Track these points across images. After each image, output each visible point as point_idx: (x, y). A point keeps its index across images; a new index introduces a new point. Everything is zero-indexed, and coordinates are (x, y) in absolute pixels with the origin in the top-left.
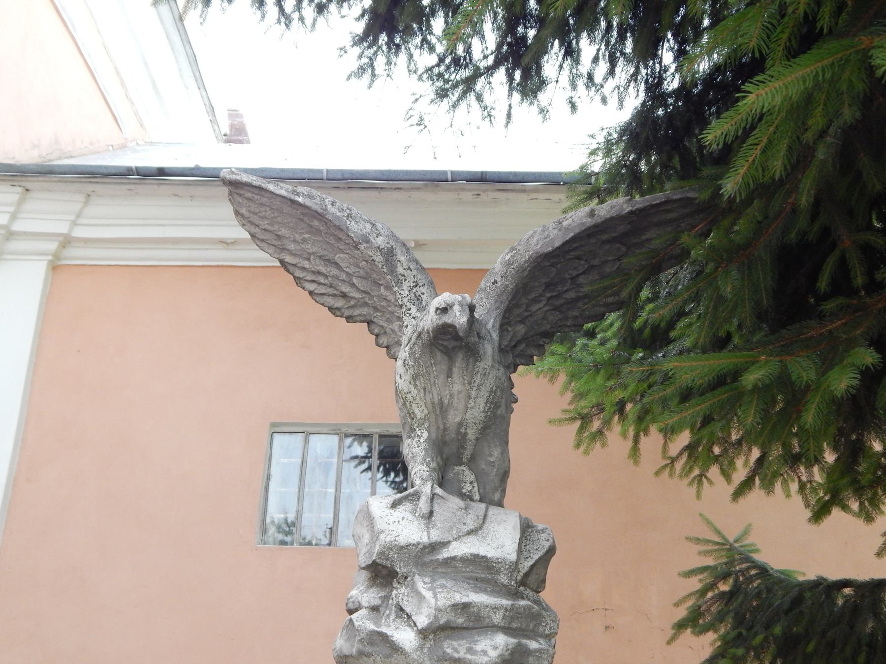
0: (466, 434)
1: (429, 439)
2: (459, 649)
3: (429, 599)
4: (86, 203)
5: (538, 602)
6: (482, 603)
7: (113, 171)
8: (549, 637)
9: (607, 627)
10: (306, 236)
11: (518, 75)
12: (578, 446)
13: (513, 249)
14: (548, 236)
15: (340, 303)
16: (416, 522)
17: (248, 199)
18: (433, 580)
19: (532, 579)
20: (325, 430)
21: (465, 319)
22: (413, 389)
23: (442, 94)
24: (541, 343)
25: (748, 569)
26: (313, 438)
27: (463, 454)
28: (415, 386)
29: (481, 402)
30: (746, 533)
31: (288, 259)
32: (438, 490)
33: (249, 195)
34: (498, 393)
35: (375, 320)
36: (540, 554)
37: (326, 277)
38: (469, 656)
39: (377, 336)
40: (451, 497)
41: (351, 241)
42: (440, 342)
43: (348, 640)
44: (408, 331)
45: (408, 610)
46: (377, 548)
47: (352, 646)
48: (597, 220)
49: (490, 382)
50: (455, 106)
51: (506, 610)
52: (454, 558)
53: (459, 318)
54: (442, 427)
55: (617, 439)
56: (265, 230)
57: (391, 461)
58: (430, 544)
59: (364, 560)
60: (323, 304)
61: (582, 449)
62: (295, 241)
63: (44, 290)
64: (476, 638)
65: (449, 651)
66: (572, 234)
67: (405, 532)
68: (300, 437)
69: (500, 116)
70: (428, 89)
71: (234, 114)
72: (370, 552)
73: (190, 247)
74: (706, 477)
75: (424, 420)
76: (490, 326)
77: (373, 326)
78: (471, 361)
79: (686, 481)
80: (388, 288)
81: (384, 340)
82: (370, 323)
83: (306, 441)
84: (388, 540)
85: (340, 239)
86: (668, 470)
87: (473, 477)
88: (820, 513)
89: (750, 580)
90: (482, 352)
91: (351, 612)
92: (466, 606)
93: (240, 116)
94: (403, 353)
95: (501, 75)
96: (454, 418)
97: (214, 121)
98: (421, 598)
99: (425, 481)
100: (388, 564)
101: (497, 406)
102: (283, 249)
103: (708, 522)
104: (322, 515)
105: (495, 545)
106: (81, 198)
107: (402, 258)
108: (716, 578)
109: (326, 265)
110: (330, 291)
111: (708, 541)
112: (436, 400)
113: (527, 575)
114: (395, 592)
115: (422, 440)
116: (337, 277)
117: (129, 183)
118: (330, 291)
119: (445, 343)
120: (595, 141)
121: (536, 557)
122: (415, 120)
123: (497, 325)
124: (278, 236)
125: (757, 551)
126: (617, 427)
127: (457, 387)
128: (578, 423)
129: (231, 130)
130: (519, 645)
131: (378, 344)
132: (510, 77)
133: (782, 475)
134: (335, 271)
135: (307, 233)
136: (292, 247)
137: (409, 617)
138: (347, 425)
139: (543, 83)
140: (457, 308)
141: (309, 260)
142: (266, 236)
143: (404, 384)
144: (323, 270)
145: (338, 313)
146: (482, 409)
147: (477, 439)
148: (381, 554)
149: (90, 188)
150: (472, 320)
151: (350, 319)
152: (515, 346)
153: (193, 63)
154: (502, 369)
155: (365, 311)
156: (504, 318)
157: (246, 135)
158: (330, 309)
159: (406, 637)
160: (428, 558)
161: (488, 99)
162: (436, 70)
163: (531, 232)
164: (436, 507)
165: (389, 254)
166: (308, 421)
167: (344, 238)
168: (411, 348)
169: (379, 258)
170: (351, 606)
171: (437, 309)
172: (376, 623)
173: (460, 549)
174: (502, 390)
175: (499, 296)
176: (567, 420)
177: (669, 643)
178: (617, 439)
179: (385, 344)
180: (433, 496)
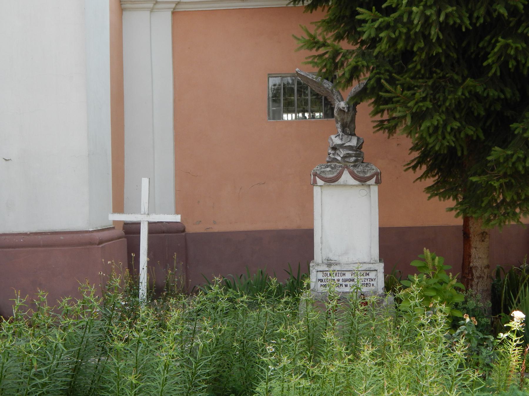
5: (360, 151)
9: (398, 145)
59: (331, 146)
96: (345, 121)
159: (339, 158)
173: (347, 144)
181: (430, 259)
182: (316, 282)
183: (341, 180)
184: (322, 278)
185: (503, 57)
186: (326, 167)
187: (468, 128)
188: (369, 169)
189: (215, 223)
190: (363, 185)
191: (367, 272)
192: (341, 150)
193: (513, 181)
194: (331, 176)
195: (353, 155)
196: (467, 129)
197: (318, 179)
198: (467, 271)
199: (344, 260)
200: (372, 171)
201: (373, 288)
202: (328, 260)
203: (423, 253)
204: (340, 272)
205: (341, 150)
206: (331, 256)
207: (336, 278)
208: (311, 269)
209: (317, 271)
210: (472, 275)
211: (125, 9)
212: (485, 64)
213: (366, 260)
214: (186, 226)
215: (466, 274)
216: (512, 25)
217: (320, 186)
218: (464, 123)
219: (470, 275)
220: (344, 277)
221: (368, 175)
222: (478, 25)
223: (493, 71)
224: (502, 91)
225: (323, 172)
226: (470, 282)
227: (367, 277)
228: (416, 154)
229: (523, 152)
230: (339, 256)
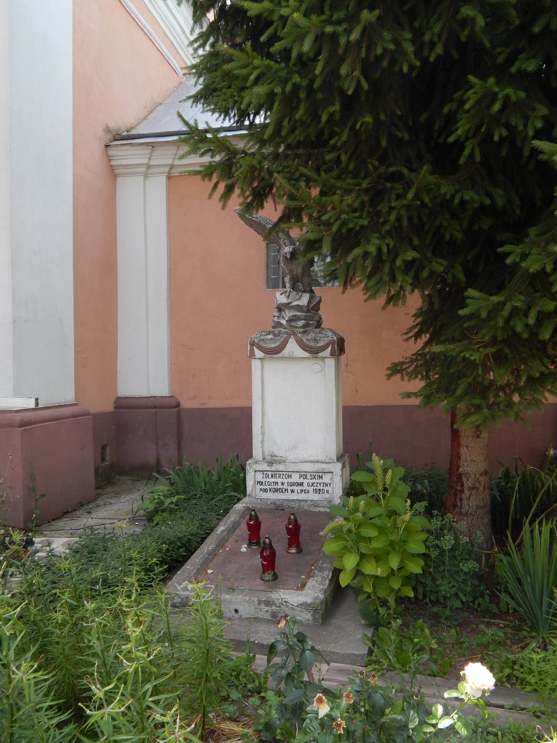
3: (288, 314)
4: (178, 149)
9: (406, 314)
29: (301, 269)
59: (275, 307)
92: (295, 315)
96: (294, 273)
106: (176, 147)
127: (294, 266)
159: (284, 322)
173: (294, 303)
180: (290, 291)
181: (379, 472)
182: (254, 486)
183: (286, 352)
184: (262, 480)
185: (484, 127)
186: (267, 335)
187: (437, 262)
188: (322, 335)
189: (210, 398)
191: (320, 475)
193: (507, 350)
194: (273, 345)
195: (302, 317)
196: (434, 263)
197: (256, 351)
198: (454, 479)
199: (292, 456)
200: (326, 339)
202: (272, 456)
203: (371, 460)
204: (285, 473)
206: (276, 451)
207: (279, 481)
208: (248, 467)
209: (256, 471)
210: (462, 485)
211: (118, 174)
212: (451, 139)
213: (321, 457)
215: (454, 482)
216: (500, 59)
217: (260, 359)
218: (429, 254)
219: (459, 485)
220: (290, 480)
221: (321, 344)
222: (432, 59)
223: (466, 152)
224: (489, 195)
225: (263, 340)
226: (459, 494)
227: (320, 481)
229: (522, 298)
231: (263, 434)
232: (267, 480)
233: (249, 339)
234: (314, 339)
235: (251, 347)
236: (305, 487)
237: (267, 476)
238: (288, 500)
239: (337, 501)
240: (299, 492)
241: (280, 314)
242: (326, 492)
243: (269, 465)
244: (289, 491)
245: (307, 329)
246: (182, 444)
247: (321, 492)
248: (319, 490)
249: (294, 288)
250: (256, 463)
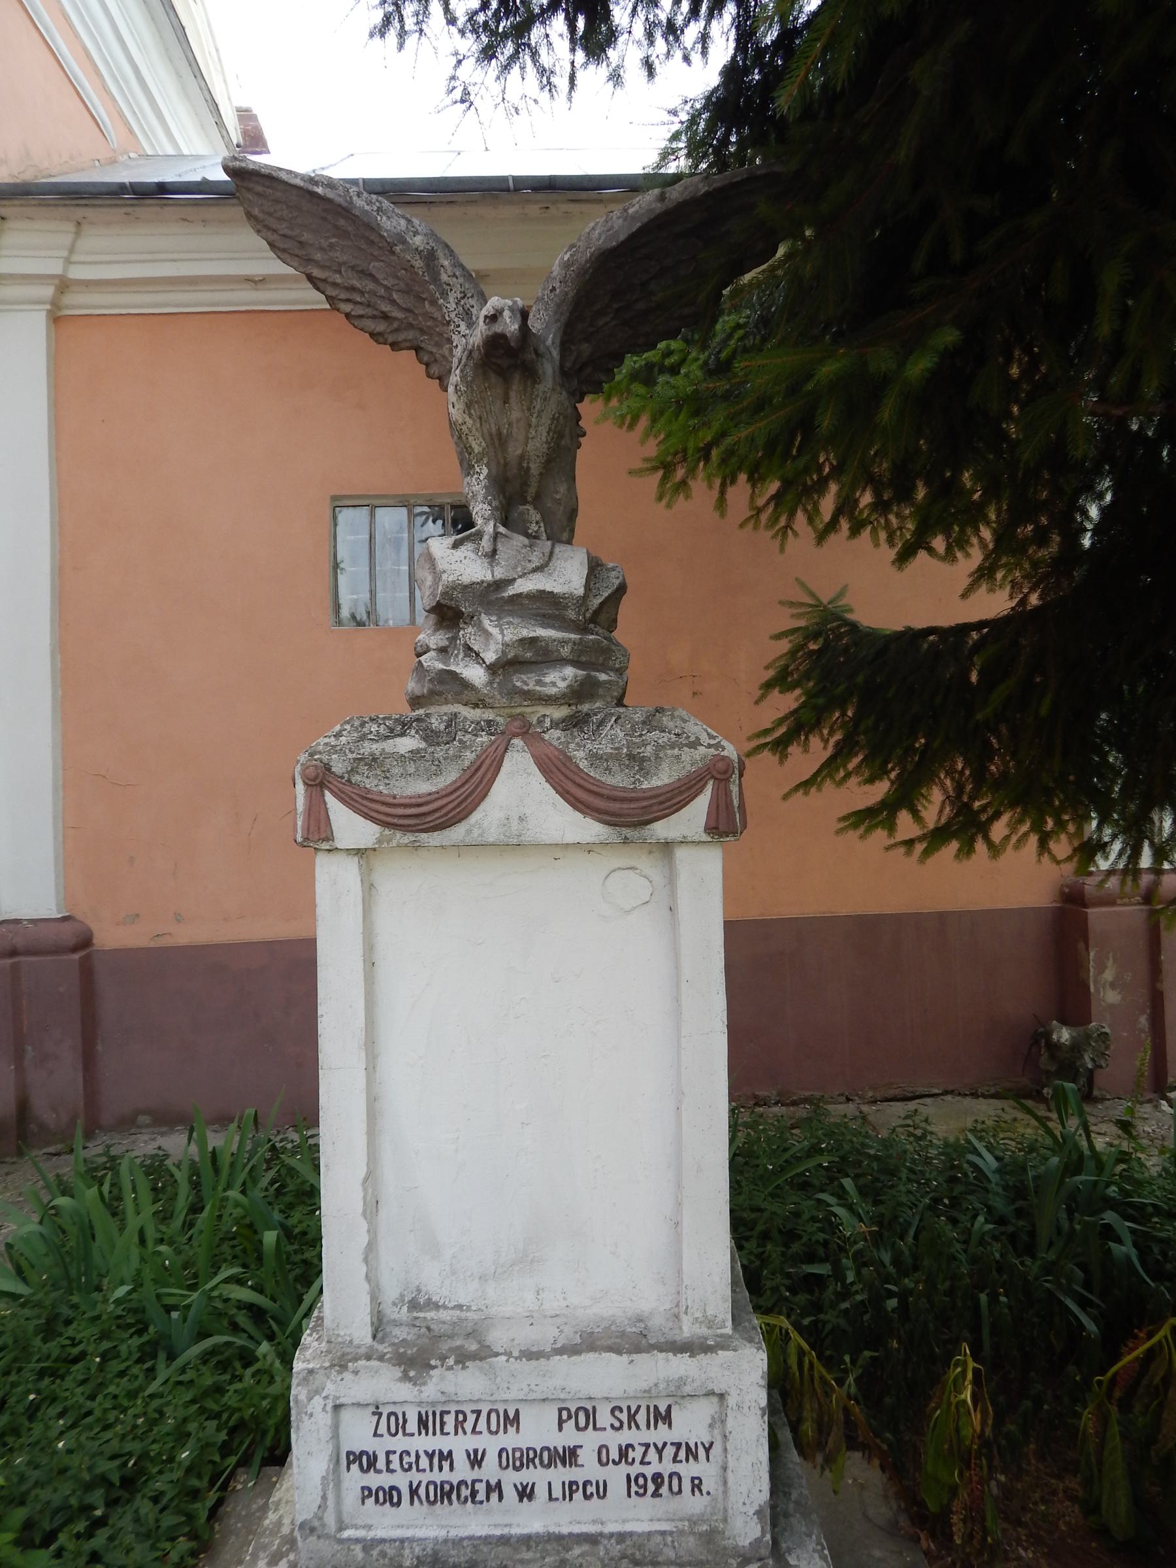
0: (529, 468)
1: (488, 476)
2: (529, 681)
3: (496, 636)
4: (78, 234)
5: (609, 639)
6: (550, 637)
7: (103, 189)
8: (620, 671)
9: (694, 694)
10: (333, 240)
11: (581, 23)
12: (660, 498)
13: (573, 246)
14: (612, 228)
15: (381, 327)
16: (479, 561)
17: (259, 194)
18: (499, 619)
19: (603, 617)
20: (391, 502)
21: (517, 326)
22: (467, 419)
23: (488, 54)
24: (610, 366)
25: (839, 627)
26: (379, 512)
27: (526, 492)
28: (470, 415)
29: (543, 430)
30: (841, 594)
31: (316, 273)
32: (502, 529)
33: (259, 189)
34: (561, 420)
35: (423, 345)
36: (610, 591)
37: (362, 293)
38: (538, 688)
39: (427, 365)
40: (515, 535)
41: (385, 244)
42: (494, 360)
43: (418, 681)
44: (458, 352)
45: (476, 648)
46: (440, 588)
47: (423, 686)
48: (668, 204)
49: (552, 408)
50: (506, 68)
51: (574, 644)
52: (520, 595)
53: (510, 326)
54: (502, 462)
55: (703, 492)
56: (284, 236)
57: (460, 522)
58: (495, 582)
60: (362, 330)
61: (664, 502)
62: (321, 249)
63: (48, 347)
64: (545, 671)
65: (518, 684)
66: (639, 224)
67: (468, 571)
68: (365, 511)
69: (561, 82)
70: (470, 45)
71: (246, 116)
72: (433, 595)
73: (211, 288)
74: (791, 529)
75: (482, 454)
76: (549, 342)
77: (421, 353)
78: (529, 383)
79: (770, 533)
80: (434, 302)
81: (435, 370)
82: (418, 349)
83: (372, 515)
84: (450, 579)
85: (372, 242)
86: (753, 521)
87: (538, 517)
88: (905, 556)
89: (840, 637)
90: (540, 372)
91: (419, 655)
92: (533, 641)
93: (254, 118)
94: (455, 378)
95: (559, 23)
96: (514, 451)
97: (220, 124)
98: (488, 635)
99: (487, 520)
100: (453, 604)
101: (561, 436)
102: (309, 261)
103: (803, 585)
104: (398, 595)
105: (561, 581)
106: (71, 227)
107: (446, 263)
108: (805, 638)
109: (360, 278)
110: (369, 311)
111: (802, 604)
112: (494, 430)
113: (597, 613)
114: (462, 632)
115: (482, 477)
116: (373, 293)
117: (127, 205)
118: (369, 311)
119: (499, 362)
120: (676, 120)
121: (606, 594)
122: (457, 94)
123: (558, 341)
124: (300, 242)
125: (851, 610)
126: (701, 473)
127: (515, 414)
128: (660, 473)
129: (244, 139)
130: (588, 676)
131: (429, 376)
132: (572, 27)
133: (871, 523)
134: (371, 286)
135: (334, 236)
136: (318, 256)
137: (477, 655)
138: (416, 496)
139: (612, 36)
140: (507, 314)
141: (340, 272)
142: (288, 244)
143: (456, 413)
144: (357, 284)
145: (381, 340)
146: (544, 439)
147: (541, 474)
148: (444, 594)
149: (80, 213)
150: (524, 327)
151: (395, 346)
152: (581, 369)
153: (182, 38)
154: (564, 393)
155: (410, 334)
156: (565, 333)
157: (265, 145)
158: (372, 335)
159: (475, 674)
160: (493, 597)
161: (545, 59)
162: (481, 18)
163: (592, 224)
164: (500, 546)
165: (430, 257)
166: (371, 493)
167: (376, 240)
168: (462, 371)
169: (418, 263)
170: (419, 649)
171: (486, 317)
172: (444, 663)
173: (525, 586)
174: (566, 417)
175: (558, 306)
176: (648, 469)
177: (756, 703)
178: (703, 492)
179: (437, 374)
180: (496, 536)
182: (333, 1479)
183: (490, 816)
186: (392, 734)
188: (664, 738)
189: (178, 918)
190: (626, 841)
192: (486, 622)
194: (422, 787)
195: (565, 651)
197: (336, 809)
200: (687, 755)
201: (693, 1504)
205: (486, 622)
206: (433, 1280)
207: (460, 1445)
208: (298, 1392)
214: (95, 927)
217: (359, 852)
220: (510, 1440)
221: (663, 777)
225: (373, 761)
227: (661, 1434)
228: (787, 702)
230: (483, 1278)
231: (372, 1208)
232: (399, 1443)
233: (303, 758)
234: (631, 757)
235: (310, 800)
236: (588, 1469)
237: (399, 1426)
238: (504, 1540)
239: (747, 1530)
240: (557, 1492)
241: (453, 640)
242: (687, 1486)
243: (405, 1377)
244: (510, 1493)
245: (585, 708)
246: (99, 1048)
247: (664, 1490)
248: (657, 1478)
249: (507, 517)
250: (343, 1368)
